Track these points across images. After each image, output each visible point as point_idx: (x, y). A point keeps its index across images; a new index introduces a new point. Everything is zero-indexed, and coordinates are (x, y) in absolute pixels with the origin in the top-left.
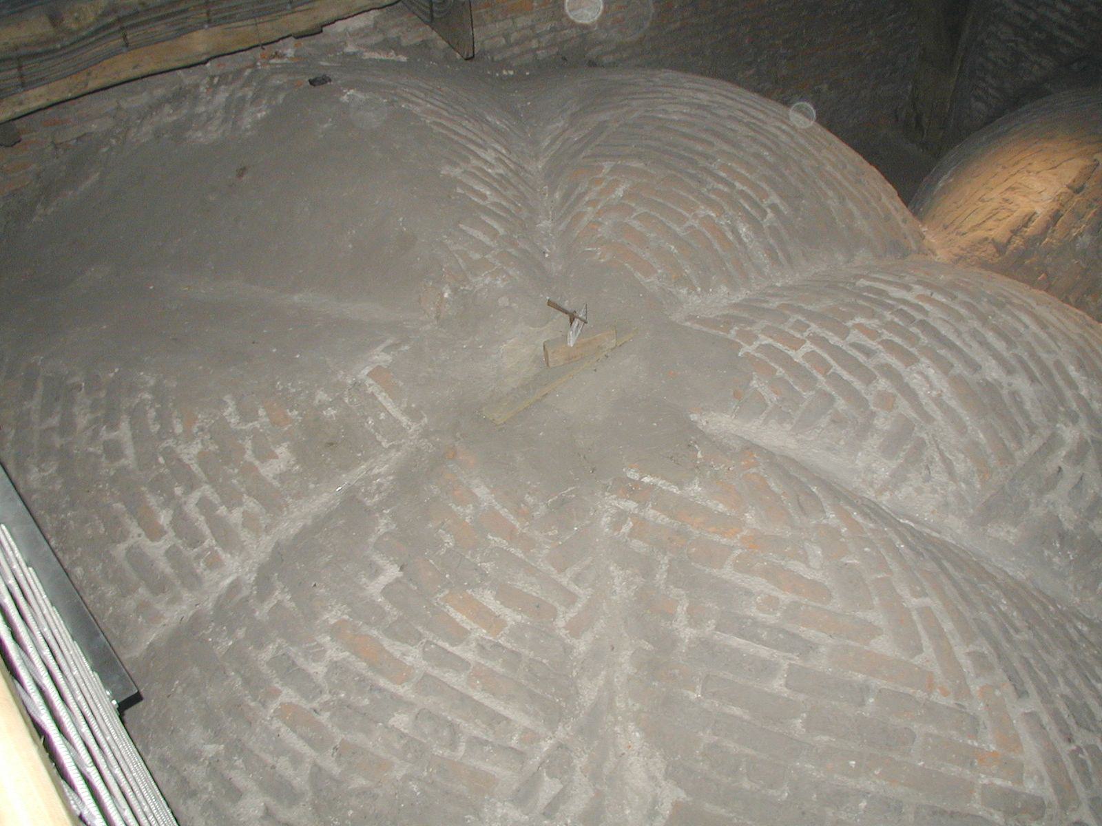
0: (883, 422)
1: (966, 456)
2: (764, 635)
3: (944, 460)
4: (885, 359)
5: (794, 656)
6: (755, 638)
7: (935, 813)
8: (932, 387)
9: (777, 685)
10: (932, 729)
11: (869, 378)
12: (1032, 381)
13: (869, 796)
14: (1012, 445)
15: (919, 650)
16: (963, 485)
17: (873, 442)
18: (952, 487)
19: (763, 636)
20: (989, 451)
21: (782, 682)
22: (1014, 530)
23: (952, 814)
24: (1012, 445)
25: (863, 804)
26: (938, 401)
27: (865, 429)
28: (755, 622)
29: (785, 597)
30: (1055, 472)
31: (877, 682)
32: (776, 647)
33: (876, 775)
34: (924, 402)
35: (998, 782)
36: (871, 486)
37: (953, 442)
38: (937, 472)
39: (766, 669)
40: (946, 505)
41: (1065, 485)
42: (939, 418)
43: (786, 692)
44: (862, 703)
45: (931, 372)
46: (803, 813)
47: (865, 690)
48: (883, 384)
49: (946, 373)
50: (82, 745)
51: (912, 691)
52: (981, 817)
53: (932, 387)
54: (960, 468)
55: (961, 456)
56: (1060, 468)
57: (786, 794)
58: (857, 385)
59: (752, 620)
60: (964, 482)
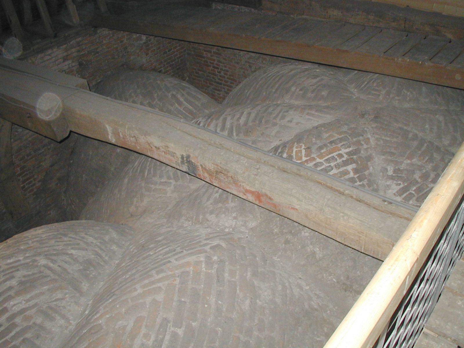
0: (39, 320)
1: (54, 293)
2: (161, 337)
3: (56, 300)
4: (4, 320)
5: (169, 325)
6: (162, 340)
7: (219, 281)
8: (21, 303)
9: (180, 332)
10: (190, 283)
11: (15, 325)
12: (19, 270)
13: (217, 300)
14: (49, 279)
15: (160, 287)
16: (67, 296)
17: (48, 324)
18: (68, 299)
19: (161, 337)
20: (52, 285)
21: (179, 330)
22: (84, 284)
23: (218, 277)
24: (49, 279)
25: (220, 302)
26: (28, 301)
27: (41, 327)
28: (156, 341)
29: (143, 330)
30: (60, 268)
31: (176, 298)
32: (166, 332)
33: (209, 298)
34: (27, 306)
35: (203, 266)
36: (67, 327)
37: (47, 297)
38: (61, 303)
39: (174, 335)
40: (75, 302)
41: (66, 266)
42: (36, 301)
43: (183, 328)
44: (185, 302)
45: (12, 303)
46: (225, 322)
47: (180, 301)
48: (18, 320)
49: (13, 298)
50: (418, 312)
51: (177, 288)
52: (217, 270)
53: (21, 303)
54: (60, 296)
55: (54, 295)
56: (58, 266)
57: (220, 328)
58: (18, 329)
59: (154, 342)
60: (66, 295)
